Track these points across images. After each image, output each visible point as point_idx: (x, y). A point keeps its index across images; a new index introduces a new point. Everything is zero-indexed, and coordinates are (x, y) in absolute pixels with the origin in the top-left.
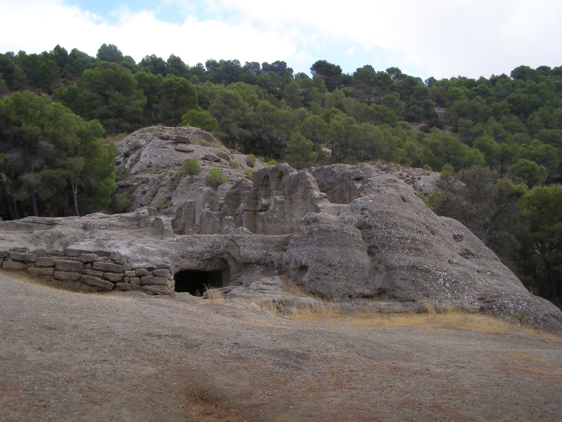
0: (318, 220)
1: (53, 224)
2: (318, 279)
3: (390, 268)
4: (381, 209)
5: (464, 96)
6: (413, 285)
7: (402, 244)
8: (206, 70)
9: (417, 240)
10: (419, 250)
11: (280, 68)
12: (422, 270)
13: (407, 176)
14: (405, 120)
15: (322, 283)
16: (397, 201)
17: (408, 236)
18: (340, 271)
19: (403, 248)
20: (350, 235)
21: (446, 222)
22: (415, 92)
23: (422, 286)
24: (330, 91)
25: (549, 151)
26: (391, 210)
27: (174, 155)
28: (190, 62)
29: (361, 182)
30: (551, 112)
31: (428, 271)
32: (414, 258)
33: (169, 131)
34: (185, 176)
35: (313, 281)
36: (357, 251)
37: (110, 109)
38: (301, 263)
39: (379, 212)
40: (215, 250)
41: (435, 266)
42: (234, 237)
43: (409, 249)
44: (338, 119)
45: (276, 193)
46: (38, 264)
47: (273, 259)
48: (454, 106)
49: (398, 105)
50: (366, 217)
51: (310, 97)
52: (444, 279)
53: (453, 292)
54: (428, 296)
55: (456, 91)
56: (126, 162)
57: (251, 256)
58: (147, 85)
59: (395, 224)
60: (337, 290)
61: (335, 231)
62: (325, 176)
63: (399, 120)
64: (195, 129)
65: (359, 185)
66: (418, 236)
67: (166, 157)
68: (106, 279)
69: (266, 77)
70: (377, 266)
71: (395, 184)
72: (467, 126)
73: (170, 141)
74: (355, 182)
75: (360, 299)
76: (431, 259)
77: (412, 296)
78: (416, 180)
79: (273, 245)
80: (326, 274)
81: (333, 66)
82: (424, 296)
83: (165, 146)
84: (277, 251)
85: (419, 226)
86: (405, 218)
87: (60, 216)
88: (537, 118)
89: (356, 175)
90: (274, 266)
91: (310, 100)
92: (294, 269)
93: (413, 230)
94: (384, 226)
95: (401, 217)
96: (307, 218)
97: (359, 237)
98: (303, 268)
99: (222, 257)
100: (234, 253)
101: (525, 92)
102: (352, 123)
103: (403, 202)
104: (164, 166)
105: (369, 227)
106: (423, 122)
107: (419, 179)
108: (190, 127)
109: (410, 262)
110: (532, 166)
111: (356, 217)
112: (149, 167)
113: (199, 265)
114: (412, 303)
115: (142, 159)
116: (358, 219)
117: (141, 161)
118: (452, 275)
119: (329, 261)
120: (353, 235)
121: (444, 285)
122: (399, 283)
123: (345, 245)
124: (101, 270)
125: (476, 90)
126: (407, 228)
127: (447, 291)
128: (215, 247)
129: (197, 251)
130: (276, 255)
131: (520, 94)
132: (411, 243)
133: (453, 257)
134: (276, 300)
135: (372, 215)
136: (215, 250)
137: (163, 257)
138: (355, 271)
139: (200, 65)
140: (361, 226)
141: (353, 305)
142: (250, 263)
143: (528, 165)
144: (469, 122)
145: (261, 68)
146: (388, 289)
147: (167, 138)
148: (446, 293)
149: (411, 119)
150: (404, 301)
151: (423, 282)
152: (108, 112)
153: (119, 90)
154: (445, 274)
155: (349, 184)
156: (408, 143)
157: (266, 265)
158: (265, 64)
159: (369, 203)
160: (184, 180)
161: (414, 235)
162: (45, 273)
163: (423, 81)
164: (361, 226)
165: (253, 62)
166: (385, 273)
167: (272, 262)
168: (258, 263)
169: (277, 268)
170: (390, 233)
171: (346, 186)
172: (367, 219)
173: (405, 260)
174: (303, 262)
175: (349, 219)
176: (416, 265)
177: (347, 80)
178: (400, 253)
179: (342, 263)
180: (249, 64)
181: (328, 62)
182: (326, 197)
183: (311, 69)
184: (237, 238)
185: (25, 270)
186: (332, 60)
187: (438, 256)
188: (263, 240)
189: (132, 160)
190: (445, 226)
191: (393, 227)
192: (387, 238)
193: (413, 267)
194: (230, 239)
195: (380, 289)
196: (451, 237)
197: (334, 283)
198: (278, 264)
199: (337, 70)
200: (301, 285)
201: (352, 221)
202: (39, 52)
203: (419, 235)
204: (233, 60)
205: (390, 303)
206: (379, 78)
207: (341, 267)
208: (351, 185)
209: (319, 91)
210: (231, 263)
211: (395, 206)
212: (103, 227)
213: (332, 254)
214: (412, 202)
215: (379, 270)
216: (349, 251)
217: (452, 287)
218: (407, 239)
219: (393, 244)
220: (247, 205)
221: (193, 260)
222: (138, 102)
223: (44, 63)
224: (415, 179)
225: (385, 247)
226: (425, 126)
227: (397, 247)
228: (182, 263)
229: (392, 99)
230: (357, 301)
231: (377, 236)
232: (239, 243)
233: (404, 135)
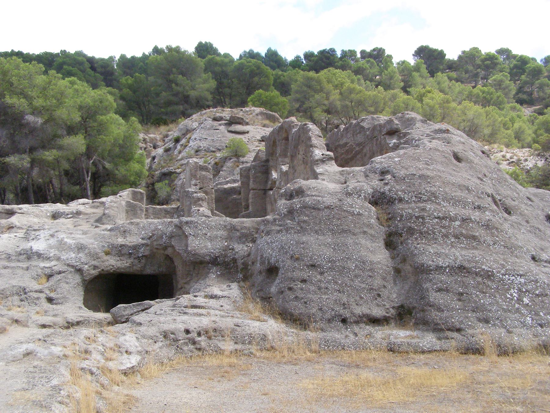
1: (11, 213)
2: (290, 289)
3: (422, 270)
4: (412, 171)
6: (460, 300)
7: (444, 227)
8: (304, 62)
9: (472, 222)
10: (474, 238)
11: (378, 56)
12: (477, 274)
13: (511, 158)
14: (517, 102)
15: (296, 297)
16: (444, 159)
17: (455, 214)
18: (329, 275)
19: (446, 236)
20: (353, 214)
21: (535, 195)
23: (475, 302)
24: (433, 76)
26: (429, 173)
27: (226, 137)
28: (288, 54)
29: (396, 137)
31: (489, 275)
32: (463, 253)
33: (227, 113)
34: (230, 159)
36: (363, 242)
37: (174, 95)
38: (269, 262)
39: (407, 176)
41: (503, 265)
42: (181, 222)
43: (456, 237)
44: (432, 99)
49: (507, 87)
50: (386, 184)
51: (410, 83)
52: (520, 290)
53: (537, 314)
54: (486, 321)
56: (176, 148)
57: (204, 251)
58: (218, 69)
59: (433, 194)
60: (321, 309)
61: (328, 207)
62: (353, 135)
63: (508, 103)
64: (258, 110)
65: (394, 141)
66: (476, 215)
67: (217, 140)
69: (363, 64)
70: (399, 266)
71: (445, 135)
73: (223, 122)
74: (387, 137)
75: (362, 325)
76: (496, 253)
77: (455, 321)
78: (522, 162)
79: (238, 234)
80: (304, 281)
81: (436, 50)
82: (479, 320)
83: (217, 128)
84: (244, 243)
85: (479, 198)
86: (453, 184)
87: (23, 204)
89: (388, 127)
91: (410, 86)
92: (260, 272)
93: (465, 204)
94: (414, 199)
95: (446, 183)
96: (289, 188)
97: (370, 217)
98: (272, 271)
99: (166, 253)
100: (179, 247)
103: (455, 162)
104: (214, 150)
108: (253, 108)
109: (456, 259)
111: (373, 184)
112: (197, 151)
113: (133, 265)
114: (455, 335)
116: (373, 189)
118: (536, 281)
119: (311, 258)
120: (359, 214)
121: (519, 300)
122: (434, 297)
123: (344, 231)
126: (456, 202)
127: (524, 311)
129: (130, 244)
132: (460, 226)
133: (542, 250)
134: (191, 329)
135: (396, 181)
137: (79, 253)
138: (356, 276)
139: (298, 57)
140: (378, 200)
141: (346, 336)
142: (201, 263)
145: (359, 56)
146: (414, 308)
147: (221, 119)
148: (523, 315)
149: (521, 102)
150: (441, 330)
151: (477, 296)
152: (172, 98)
153: (183, 75)
154: (522, 280)
155: (380, 142)
156: (516, 125)
158: (363, 52)
159: (394, 162)
160: (229, 164)
161: (467, 212)
163: (538, 61)
164: (378, 200)
165: (349, 50)
166: (412, 279)
167: (235, 260)
168: (214, 261)
169: (242, 270)
170: (424, 210)
171: (376, 144)
172: (387, 188)
173: (446, 255)
174: (273, 261)
175: (355, 188)
176: (467, 265)
177: (452, 66)
178: (440, 245)
179: (335, 262)
180: (346, 52)
181: (431, 46)
182: (330, 159)
183: (413, 55)
184: (187, 223)
186: (433, 45)
187: (511, 248)
188: (225, 226)
190: (532, 201)
191: (429, 200)
193: (461, 268)
194: (176, 226)
195: (402, 306)
196: (542, 217)
197: (315, 297)
198: (243, 264)
199: (441, 54)
200: (266, 299)
201: (360, 191)
202: (139, 55)
203: (477, 213)
204: (328, 49)
205: (415, 333)
206: (486, 59)
207: (331, 269)
208: (383, 142)
209: (420, 76)
210: (178, 263)
211: (439, 167)
212: (69, 216)
213: (318, 245)
214: (471, 162)
215: (402, 274)
216: (350, 240)
217: (535, 304)
218: (452, 219)
219: (428, 228)
222: (206, 86)
223: (141, 64)
225: (412, 234)
227: (434, 233)
228: (103, 262)
229: (501, 81)
230: (356, 329)
232: (188, 230)
233: (513, 118)
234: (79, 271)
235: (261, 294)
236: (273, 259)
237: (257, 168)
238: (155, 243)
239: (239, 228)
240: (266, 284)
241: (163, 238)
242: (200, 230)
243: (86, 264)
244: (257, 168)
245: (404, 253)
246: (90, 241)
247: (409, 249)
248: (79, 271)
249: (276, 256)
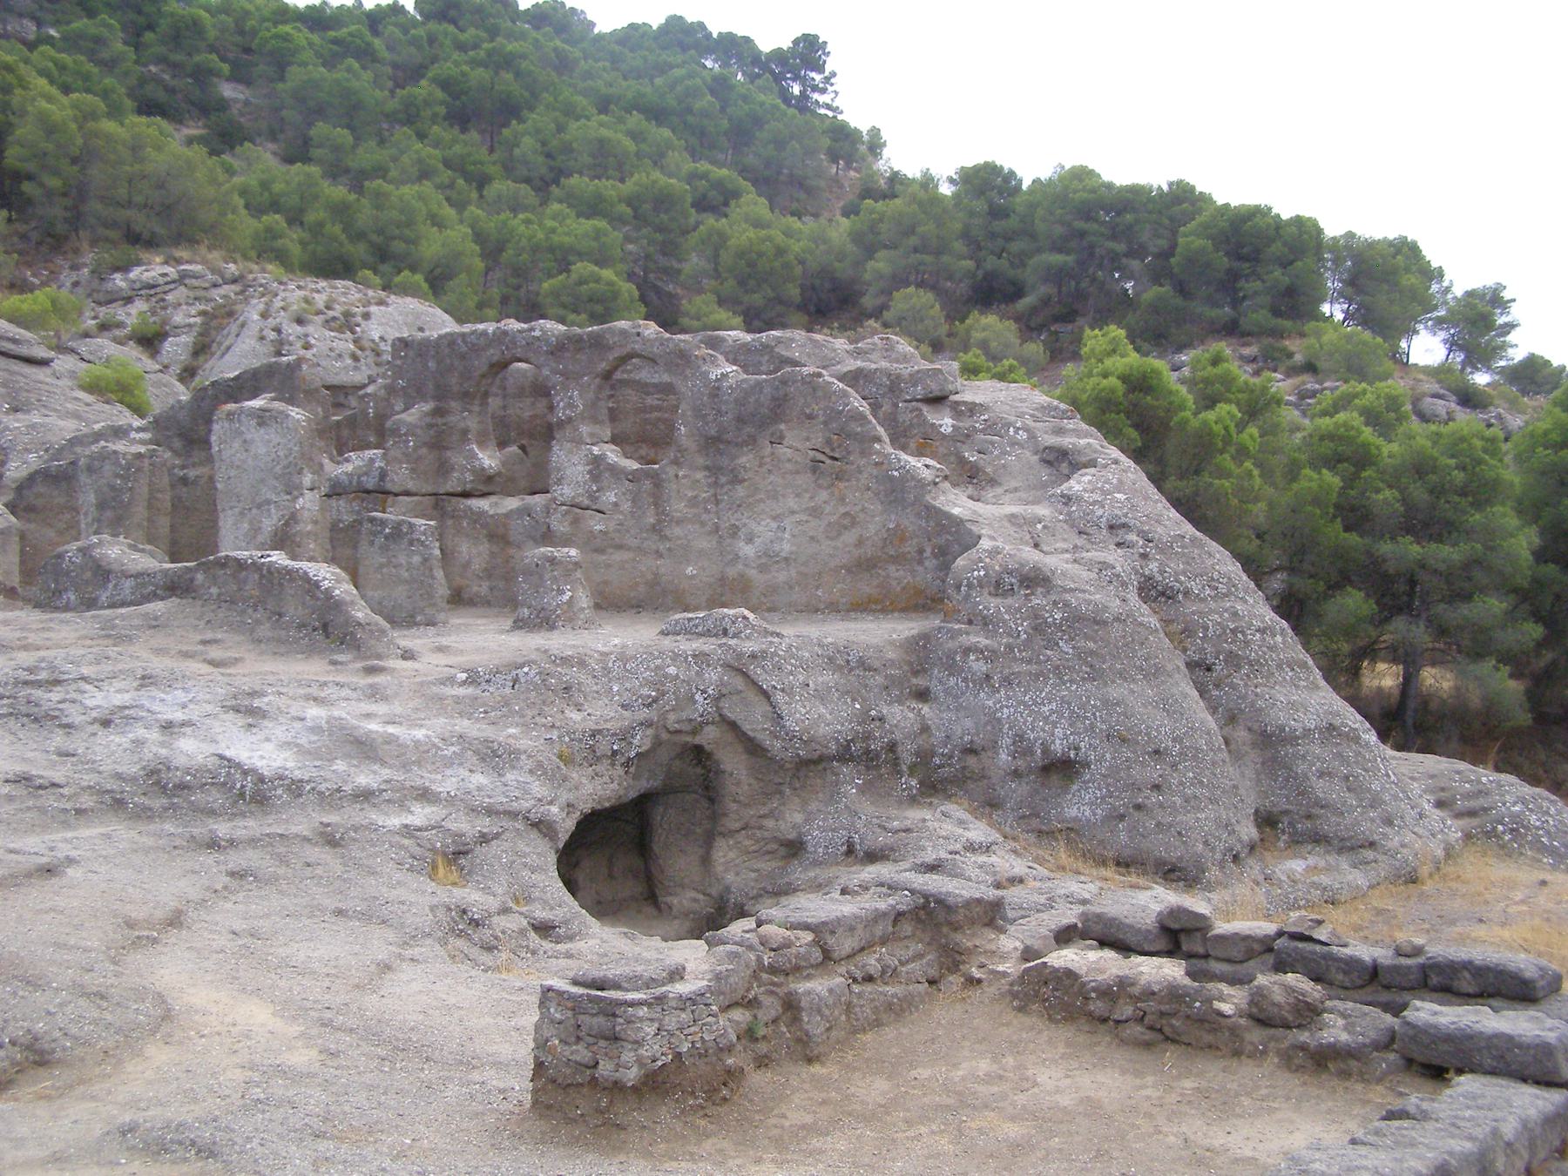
2: (1138, 807)
5: (307, 55)
15: (1158, 824)
22: (164, 25)
25: (603, 239)
30: (561, 129)
35: (1122, 817)
40: (672, 717)
42: (740, 655)
45: (592, 435)
47: (898, 736)
48: (289, 84)
55: (286, 38)
57: (823, 730)
72: (337, 149)
74: (925, 408)
78: (359, 319)
79: (879, 679)
84: (900, 702)
88: (528, 142)
90: (896, 762)
92: (1016, 774)
98: (1062, 769)
99: (697, 740)
100: (754, 720)
101: (475, 63)
102: (92, 115)
105: (1163, 594)
106: (191, 123)
107: (367, 316)
110: (610, 284)
119: (1147, 734)
125: (335, 41)
128: (670, 700)
130: (901, 716)
131: (465, 68)
143: (597, 281)
144: (343, 135)
157: (868, 759)
168: (845, 755)
169: (912, 769)
174: (1058, 747)
184: (753, 656)
192: (1234, 631)
194: (728, 666)
198: (917, 754)
220: (413, 470)
221: (598, 768)
224: (354, 315)
225: (1238, 667)
231: (1206, 629)
234: (542, 826)
235: (1035, 823)
236: (1058, 742)
237: (419, 431)
238: (672, 717)
239: (877, 664)
240: (1045, 800)
241: (695, 702)
242: (791, 673)
243: (551, 803)
244: (419, 431)
245: (1232, 705)
246: (127, 697)
247: (1244, 698)
248: (542, 826)
249: (1066, 737)
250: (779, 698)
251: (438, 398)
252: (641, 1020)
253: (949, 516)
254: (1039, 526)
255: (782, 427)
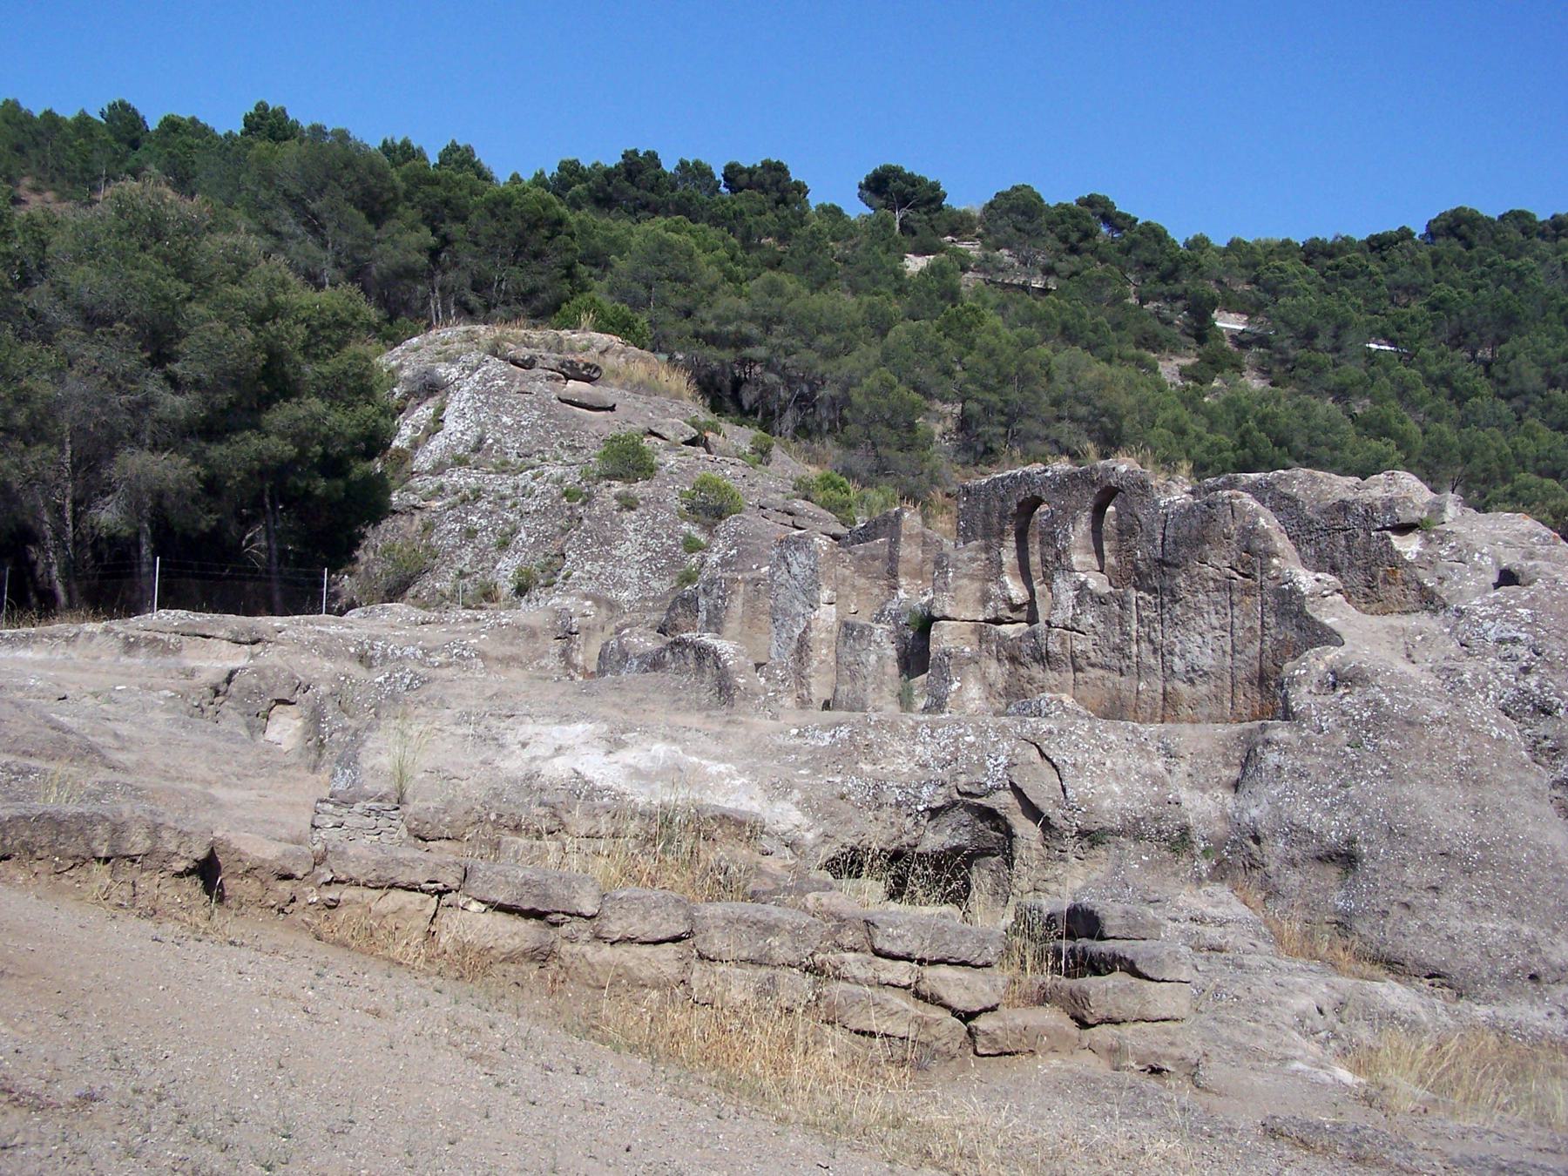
0: (1366, 680)
20: (1490, 740)
46: (615, 928)
50: (1526, 670)
68: (935, 1000)
100: (1042, 791)
115: (451, 424)
117: (446, 431)
124: (908, 958)
136: (963, 778)
162: (646, 973)
172: (1532, 681)
185: (541, 956)
189: (416, 428)
226: (1194, 366)
238: (963, 778)
250: (1068, 771)
251: (985, 536)
252: (325, 812)
253: (1322, 626)
254: (1419, 638)
255: (1207, 547)
